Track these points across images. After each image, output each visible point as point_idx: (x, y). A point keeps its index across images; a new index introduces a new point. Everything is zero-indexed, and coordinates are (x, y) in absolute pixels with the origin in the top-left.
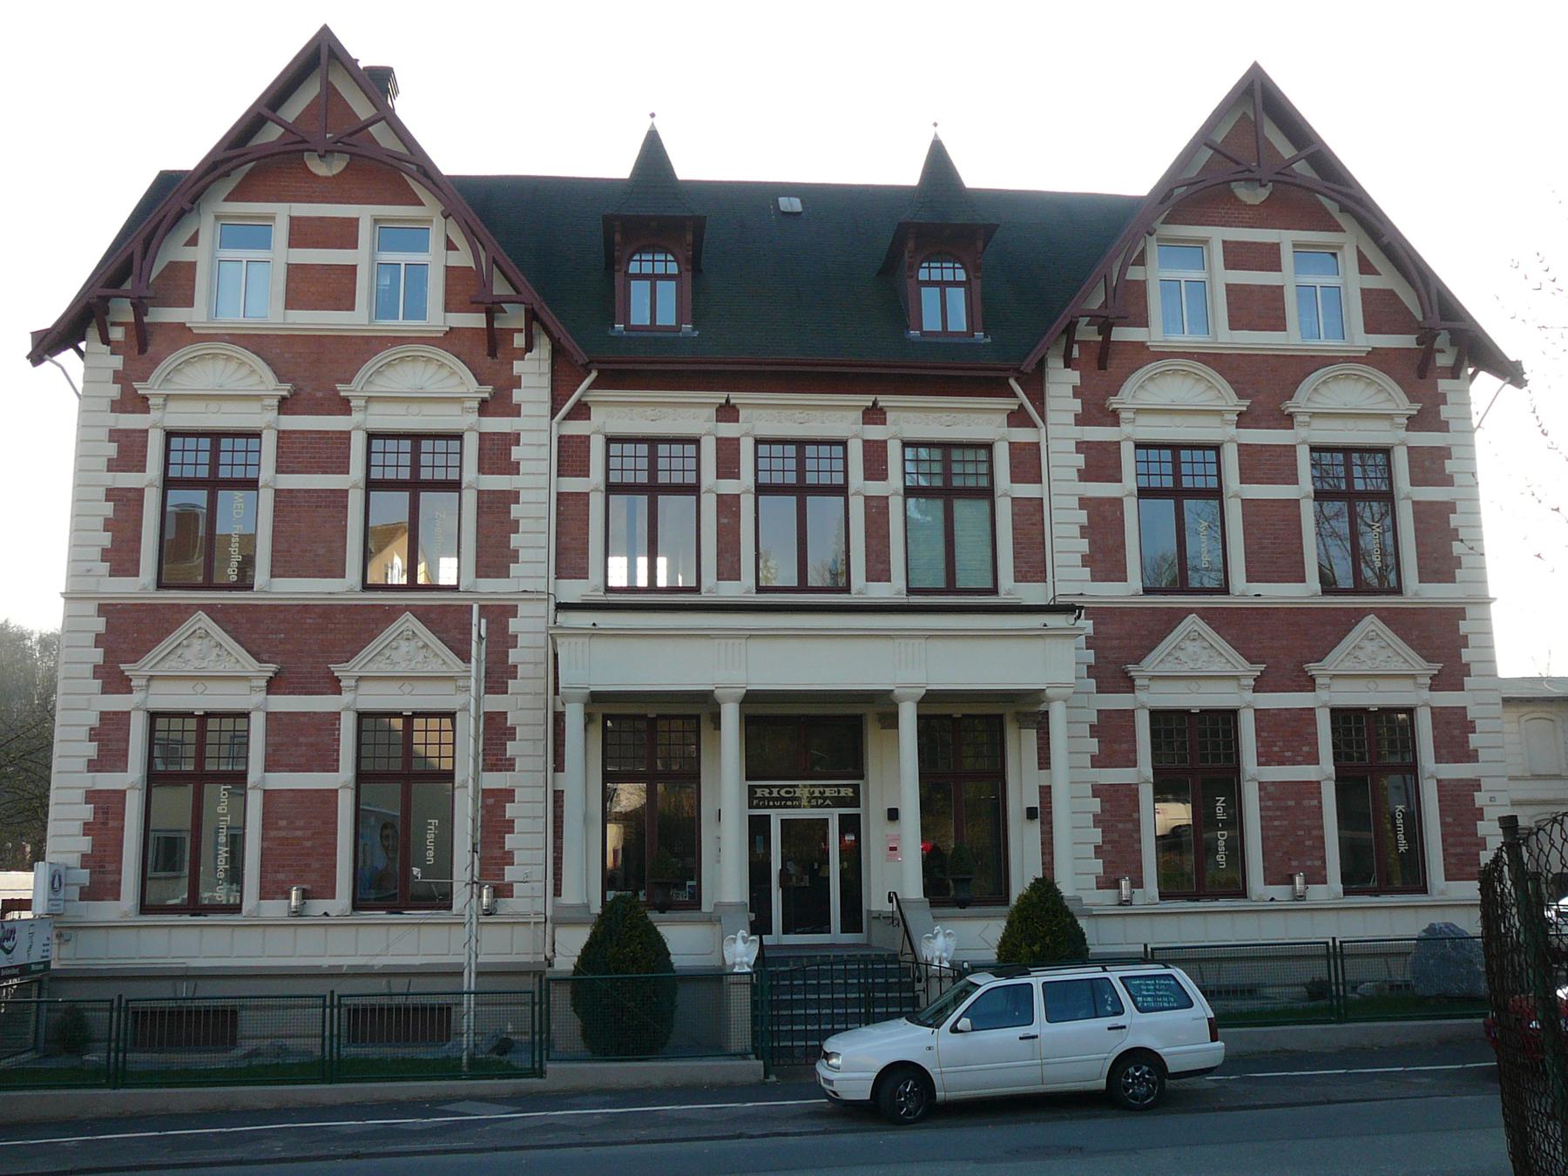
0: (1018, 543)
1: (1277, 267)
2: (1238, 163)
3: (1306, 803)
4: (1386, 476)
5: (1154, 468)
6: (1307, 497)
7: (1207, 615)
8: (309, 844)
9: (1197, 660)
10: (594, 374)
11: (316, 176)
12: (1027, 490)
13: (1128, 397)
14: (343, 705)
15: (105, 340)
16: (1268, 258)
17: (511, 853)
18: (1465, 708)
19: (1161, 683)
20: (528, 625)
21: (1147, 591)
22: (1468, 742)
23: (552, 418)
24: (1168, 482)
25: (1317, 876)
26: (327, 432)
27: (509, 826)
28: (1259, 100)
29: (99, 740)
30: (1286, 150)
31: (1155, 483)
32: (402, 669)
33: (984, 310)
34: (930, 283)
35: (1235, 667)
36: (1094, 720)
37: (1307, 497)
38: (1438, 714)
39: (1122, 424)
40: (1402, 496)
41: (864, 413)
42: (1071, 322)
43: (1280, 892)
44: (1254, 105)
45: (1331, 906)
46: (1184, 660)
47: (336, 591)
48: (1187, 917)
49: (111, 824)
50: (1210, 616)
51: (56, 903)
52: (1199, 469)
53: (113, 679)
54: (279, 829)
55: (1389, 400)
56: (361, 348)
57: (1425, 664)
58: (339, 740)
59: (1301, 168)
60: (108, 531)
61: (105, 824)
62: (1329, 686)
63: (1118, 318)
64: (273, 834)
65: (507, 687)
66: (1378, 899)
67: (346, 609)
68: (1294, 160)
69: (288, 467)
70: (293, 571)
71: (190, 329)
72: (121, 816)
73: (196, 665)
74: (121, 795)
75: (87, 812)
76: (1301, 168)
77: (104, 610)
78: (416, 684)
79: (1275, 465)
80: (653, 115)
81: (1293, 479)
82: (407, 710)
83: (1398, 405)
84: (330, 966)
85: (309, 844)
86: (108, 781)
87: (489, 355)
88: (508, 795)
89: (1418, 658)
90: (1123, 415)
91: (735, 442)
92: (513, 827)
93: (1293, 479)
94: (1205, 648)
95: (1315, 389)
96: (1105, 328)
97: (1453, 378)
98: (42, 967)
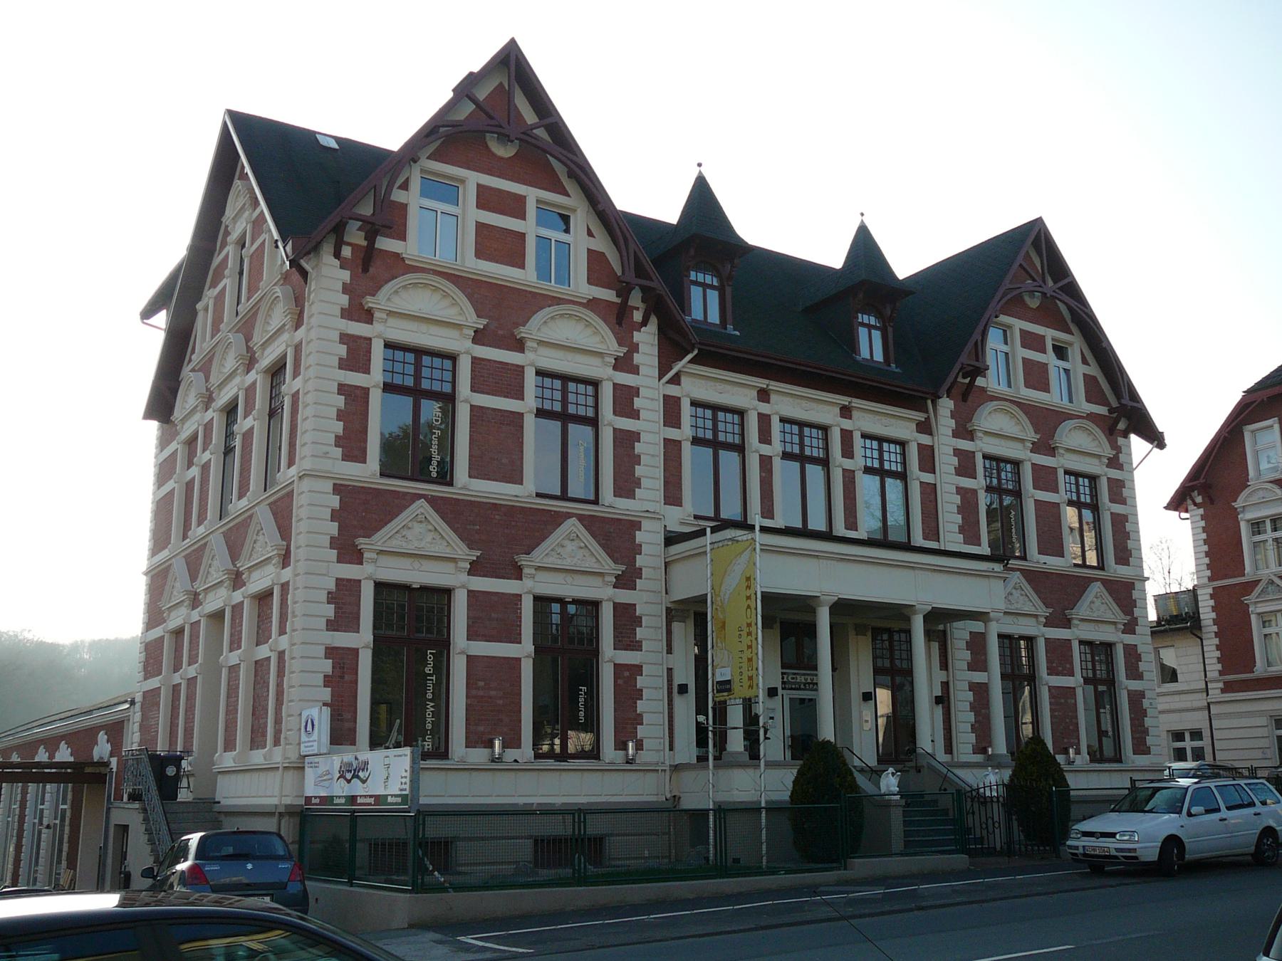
0: (924, 513)
1: (522, 215)
2: (491, 118)
3: (1069, 701)
4: (1017, 480)
5: (398, 368)
6: (530, 412)
7: (433, 501)
8: (501, 702)
9: (421, 540)
10: (696, 352)
11: (493, 154)
12: (927, 478)
13: (379, 301)
14: (526, 588)
15: (337, 255)
16: (515, 207)
17: (640, 716)
18: (1136, 645)
19: (1086, 624)
20: (649, 538)
21: (538, 495)
22: (1138, 667)
23: (659, 380)
24: (409, 382)
25: (513, 741)
26: (507, 364)
27: (639, 694)
28: (513, 68)
29: (335, 603)
30: (530, 117)
31: (398, 380)
32: (567, 563)
33: (895, 345)
34: (696, 283)
35: (456, 550)
36: (332, 586)
37: (778, 455)
38: (618, 607)
39: (526, 351)
40: (462, 399)
41: (758, 391)
42: (341, 221)
43: (479, 755)
44: (509, 73)
45: (432, 766)
46: (1013, 602)
47: (520, 495)
48: (546, 773)
49: (347, 677)
50: (436, 503)
51: (309, 744)
52: (437, 374)
53: (348, 550)
54: (478, 689)
55: (602, 342)
56: (531, 302)
57: (613, 565)
58: (521, 617)
59: (541, 133)
60: (341, 421)
61: (342, 677)
62: (533, 577)
63: (383, 226)
64: (474, 692)
65: (635, 585)
66: (1100, 765)
67: (523, 510)
68: (536, 126)
69: (479, 388)
70: (486, 475)
71: (403, 259)
72: (355, 671)
73: (416, 545)
74: (355, 652)
75: (327, 666)
76: (541, 133)
77: (337, 489)
78: (576, 577)
79: (509, 381)
80: (862, 214)
81: (520, 396)
82: (1097, 640)
83: (608, 347)
84: (525, 804)
85: (501, 702)
86: (343, 639)
87: (617, 323)
88: (637, 669)
89: (1042, 605)
90: (377, 315)
91: (971, 455)
92: (642, 695)
93: (520, 396)
94: (581, 548)
95: (545, 322)
96: (371, 237)
97: (1124, 437)
98: (399, 800)
